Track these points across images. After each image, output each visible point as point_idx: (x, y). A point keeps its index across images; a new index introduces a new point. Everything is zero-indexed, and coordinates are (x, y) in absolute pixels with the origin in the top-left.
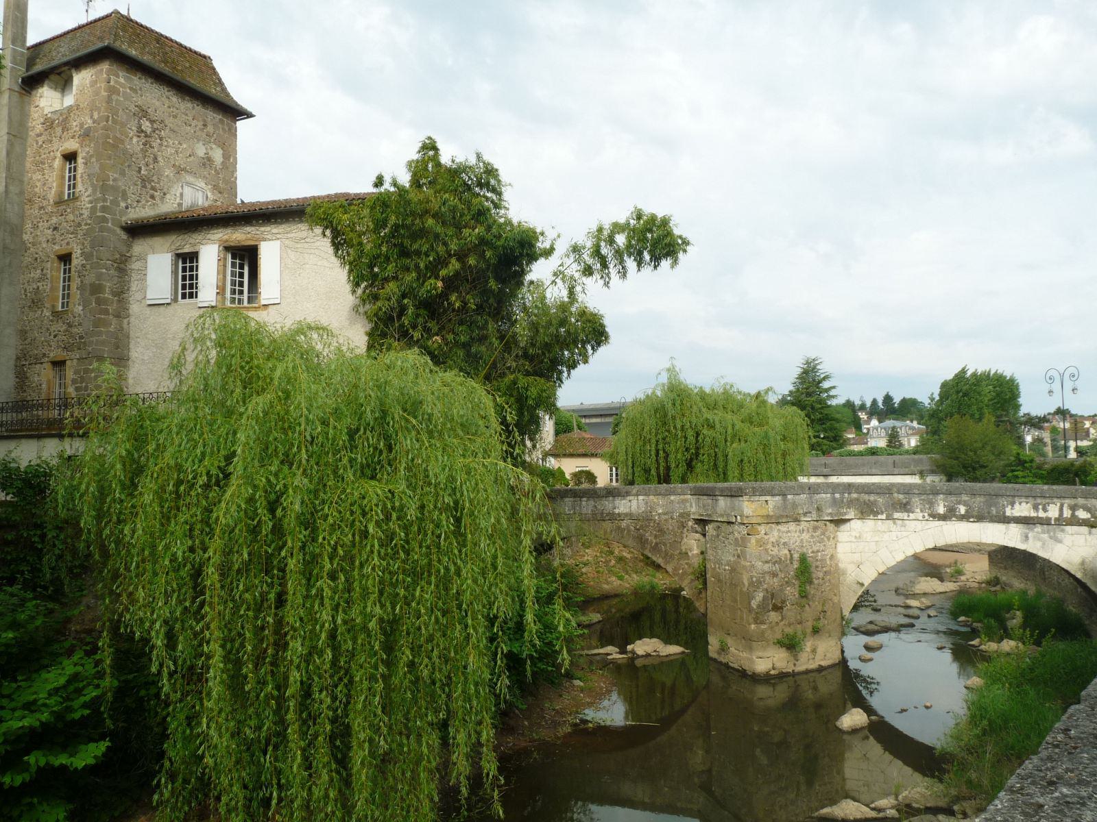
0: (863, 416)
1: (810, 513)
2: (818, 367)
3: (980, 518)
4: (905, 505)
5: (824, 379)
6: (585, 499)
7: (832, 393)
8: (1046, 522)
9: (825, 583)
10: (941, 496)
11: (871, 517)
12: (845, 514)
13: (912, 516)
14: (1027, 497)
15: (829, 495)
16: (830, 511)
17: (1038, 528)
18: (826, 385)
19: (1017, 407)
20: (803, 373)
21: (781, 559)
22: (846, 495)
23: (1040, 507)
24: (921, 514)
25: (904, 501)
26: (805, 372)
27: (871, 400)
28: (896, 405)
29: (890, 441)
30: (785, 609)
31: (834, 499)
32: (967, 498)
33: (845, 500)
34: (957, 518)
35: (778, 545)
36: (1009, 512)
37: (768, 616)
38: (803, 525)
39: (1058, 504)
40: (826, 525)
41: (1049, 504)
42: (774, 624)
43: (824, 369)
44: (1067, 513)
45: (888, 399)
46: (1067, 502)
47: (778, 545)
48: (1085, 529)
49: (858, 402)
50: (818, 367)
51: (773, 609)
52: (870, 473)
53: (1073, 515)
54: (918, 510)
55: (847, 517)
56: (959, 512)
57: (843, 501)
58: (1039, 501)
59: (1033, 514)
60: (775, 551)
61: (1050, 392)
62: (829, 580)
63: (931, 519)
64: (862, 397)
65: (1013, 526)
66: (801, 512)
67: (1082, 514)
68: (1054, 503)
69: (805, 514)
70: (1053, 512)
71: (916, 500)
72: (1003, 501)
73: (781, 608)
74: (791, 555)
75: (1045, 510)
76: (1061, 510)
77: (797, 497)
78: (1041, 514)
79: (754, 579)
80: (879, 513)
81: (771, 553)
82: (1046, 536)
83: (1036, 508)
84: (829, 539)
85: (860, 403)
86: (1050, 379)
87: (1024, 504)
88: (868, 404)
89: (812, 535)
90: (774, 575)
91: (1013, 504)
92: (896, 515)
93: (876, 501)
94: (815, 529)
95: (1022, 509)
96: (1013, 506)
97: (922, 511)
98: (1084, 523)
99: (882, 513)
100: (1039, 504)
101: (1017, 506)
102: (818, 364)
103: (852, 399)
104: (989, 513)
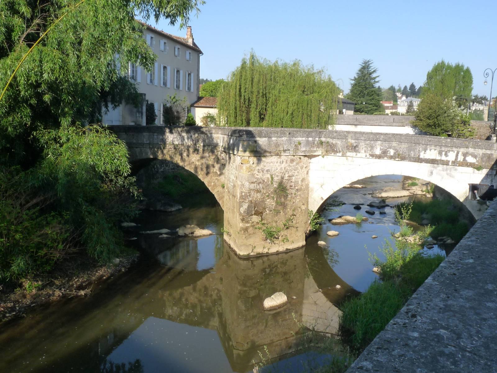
0: (399, 95)
1: (289, 150)
2: (371, 65)
3: (403, 158)
4: (355, 147)
5: (374, 71)
6: (156, 134)
7: (377, 80)
8: (446, 163)
9: (296, 196)
10: (379, 142)
11: (333, 154)
12: (315, 151)
13: (359, 155)
14: (436, 146)
15: (304, 139)
16: (304, 149)
17: (441, 167)
18: (374, 75)
19: (471, 90)
20: (362, 68)
21: (264, 181)
22: (317, 139)
23: (444, 153)
24: (365, 154)
25: (355, 145)
26: (364, 68)
27: (404, 86)
28: (416, 90)
29: (408, 109)
30: (264, 214)
31: (308, 141)
32: (396, 145)
33: (316, 142)
34: (387, 158)
35: (263, 171)
36: (422, 156)
37: (251, 218)
38: (283, 158)
39: (456, 152)
40: (300, 158)
41: (449, 151)
42: (255, 223)
43: (373, 67)
44: (461, 158)
45: (412, 86)
46: (462, 150)
47: (263, 171)
48: (470, 169)
49: (397, 88)
50: (371, 65)
51: (255, 214)
52: (380, 124)
53: (464, 159)
54: (363, 151)
55: (316, 154)
56: (390, 153)
57: (314, 143)
58: (443, 149)
59: (438, 158)
60: (260, 175)
61: (486, 82)
62: (300, 195)
63: (371, 157)
64: (399, 85)
65: (423, 164)
66: (282, 149)
67: (470, 159)
68: (453, 151)
69: (285, 151)
70: (451, 157)
71: (362, 145)
72: (420, 148)
73: (262, 213)
74: (272, 178)
75: (446, 155)
76: (457, 156)
77: (280, 139)
78: (444, 158)
79: (243, 194)
80: (337, 152)
81: (257, 176)
82: (444, 173)
83: (440, 153)
84: (302, 168)
85: (398, 88)
86: (487, 74)
87: (433, 150)
88: (402, 89)
89: (289, 165)
90: (258, 191)
91: (425, 150)
92: (349, 154)
93: (336, 144)
94: (292, 161)
95: (432, 154)
96: (425, 151)
97: (365, 152)
98: (471, 165)
99: (340, 152)
100: (443, 151)
101: (428, 151)
102: (370, 64)
103: (394, 86)
104: (409, 155)
